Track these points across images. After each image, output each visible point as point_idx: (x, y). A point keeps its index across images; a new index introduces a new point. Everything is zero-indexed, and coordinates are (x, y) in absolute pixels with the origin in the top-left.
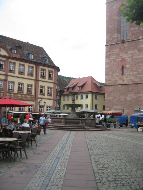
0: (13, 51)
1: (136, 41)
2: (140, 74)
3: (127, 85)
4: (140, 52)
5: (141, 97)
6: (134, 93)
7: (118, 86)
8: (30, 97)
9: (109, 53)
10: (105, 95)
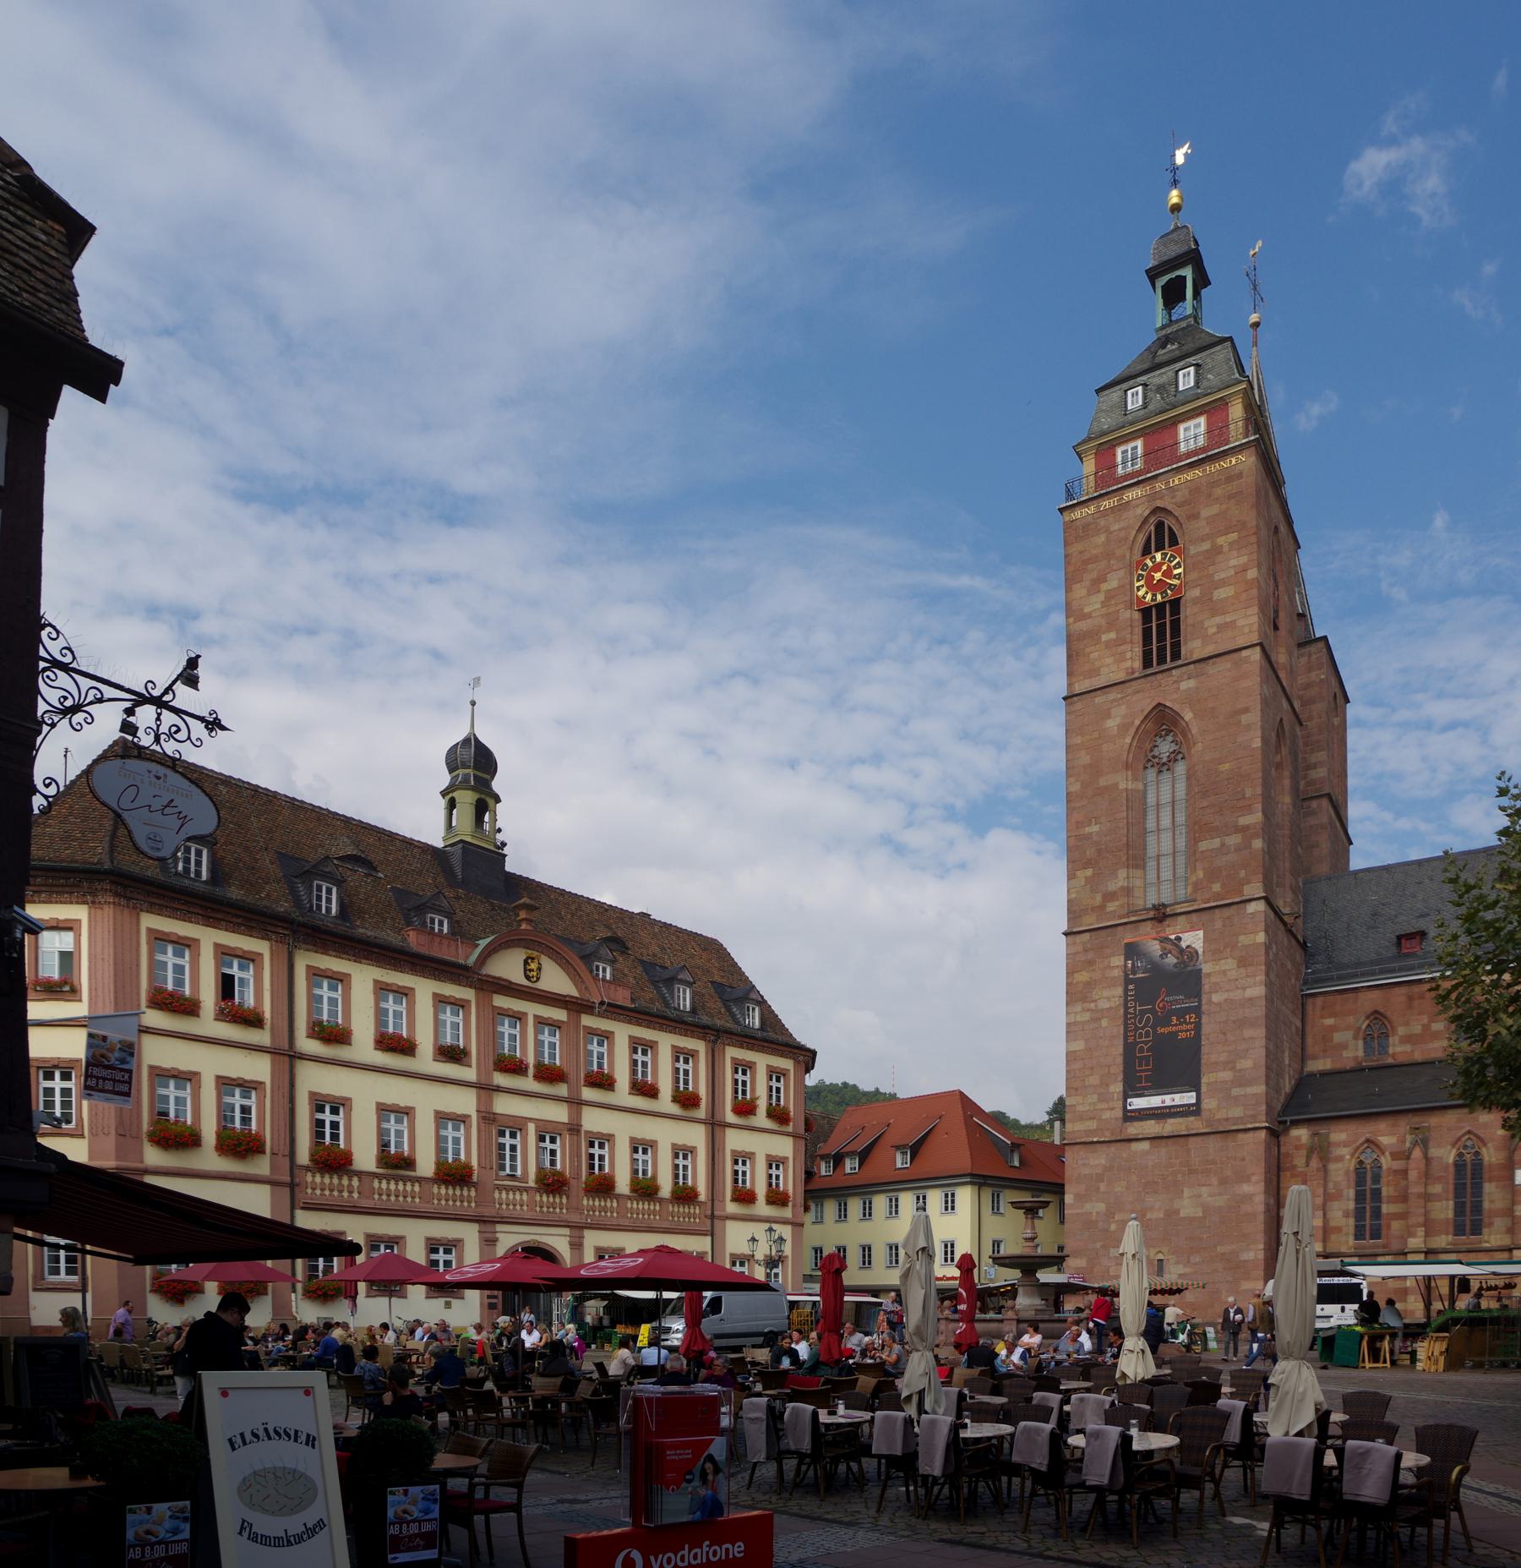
0: (433, 921)
1: (1227, 912)
2: (1250, 1083)
3: (1182, 1140)
4: (1250, 969)
5: (1249, 1198)
6: (1215, 1181)
7: (1134, 1146)
8: (605, 1209)
9: (1083, 977)
10: (1063, 1193)
